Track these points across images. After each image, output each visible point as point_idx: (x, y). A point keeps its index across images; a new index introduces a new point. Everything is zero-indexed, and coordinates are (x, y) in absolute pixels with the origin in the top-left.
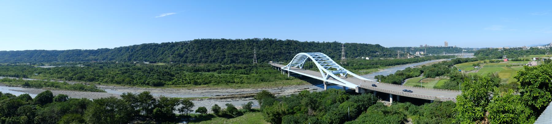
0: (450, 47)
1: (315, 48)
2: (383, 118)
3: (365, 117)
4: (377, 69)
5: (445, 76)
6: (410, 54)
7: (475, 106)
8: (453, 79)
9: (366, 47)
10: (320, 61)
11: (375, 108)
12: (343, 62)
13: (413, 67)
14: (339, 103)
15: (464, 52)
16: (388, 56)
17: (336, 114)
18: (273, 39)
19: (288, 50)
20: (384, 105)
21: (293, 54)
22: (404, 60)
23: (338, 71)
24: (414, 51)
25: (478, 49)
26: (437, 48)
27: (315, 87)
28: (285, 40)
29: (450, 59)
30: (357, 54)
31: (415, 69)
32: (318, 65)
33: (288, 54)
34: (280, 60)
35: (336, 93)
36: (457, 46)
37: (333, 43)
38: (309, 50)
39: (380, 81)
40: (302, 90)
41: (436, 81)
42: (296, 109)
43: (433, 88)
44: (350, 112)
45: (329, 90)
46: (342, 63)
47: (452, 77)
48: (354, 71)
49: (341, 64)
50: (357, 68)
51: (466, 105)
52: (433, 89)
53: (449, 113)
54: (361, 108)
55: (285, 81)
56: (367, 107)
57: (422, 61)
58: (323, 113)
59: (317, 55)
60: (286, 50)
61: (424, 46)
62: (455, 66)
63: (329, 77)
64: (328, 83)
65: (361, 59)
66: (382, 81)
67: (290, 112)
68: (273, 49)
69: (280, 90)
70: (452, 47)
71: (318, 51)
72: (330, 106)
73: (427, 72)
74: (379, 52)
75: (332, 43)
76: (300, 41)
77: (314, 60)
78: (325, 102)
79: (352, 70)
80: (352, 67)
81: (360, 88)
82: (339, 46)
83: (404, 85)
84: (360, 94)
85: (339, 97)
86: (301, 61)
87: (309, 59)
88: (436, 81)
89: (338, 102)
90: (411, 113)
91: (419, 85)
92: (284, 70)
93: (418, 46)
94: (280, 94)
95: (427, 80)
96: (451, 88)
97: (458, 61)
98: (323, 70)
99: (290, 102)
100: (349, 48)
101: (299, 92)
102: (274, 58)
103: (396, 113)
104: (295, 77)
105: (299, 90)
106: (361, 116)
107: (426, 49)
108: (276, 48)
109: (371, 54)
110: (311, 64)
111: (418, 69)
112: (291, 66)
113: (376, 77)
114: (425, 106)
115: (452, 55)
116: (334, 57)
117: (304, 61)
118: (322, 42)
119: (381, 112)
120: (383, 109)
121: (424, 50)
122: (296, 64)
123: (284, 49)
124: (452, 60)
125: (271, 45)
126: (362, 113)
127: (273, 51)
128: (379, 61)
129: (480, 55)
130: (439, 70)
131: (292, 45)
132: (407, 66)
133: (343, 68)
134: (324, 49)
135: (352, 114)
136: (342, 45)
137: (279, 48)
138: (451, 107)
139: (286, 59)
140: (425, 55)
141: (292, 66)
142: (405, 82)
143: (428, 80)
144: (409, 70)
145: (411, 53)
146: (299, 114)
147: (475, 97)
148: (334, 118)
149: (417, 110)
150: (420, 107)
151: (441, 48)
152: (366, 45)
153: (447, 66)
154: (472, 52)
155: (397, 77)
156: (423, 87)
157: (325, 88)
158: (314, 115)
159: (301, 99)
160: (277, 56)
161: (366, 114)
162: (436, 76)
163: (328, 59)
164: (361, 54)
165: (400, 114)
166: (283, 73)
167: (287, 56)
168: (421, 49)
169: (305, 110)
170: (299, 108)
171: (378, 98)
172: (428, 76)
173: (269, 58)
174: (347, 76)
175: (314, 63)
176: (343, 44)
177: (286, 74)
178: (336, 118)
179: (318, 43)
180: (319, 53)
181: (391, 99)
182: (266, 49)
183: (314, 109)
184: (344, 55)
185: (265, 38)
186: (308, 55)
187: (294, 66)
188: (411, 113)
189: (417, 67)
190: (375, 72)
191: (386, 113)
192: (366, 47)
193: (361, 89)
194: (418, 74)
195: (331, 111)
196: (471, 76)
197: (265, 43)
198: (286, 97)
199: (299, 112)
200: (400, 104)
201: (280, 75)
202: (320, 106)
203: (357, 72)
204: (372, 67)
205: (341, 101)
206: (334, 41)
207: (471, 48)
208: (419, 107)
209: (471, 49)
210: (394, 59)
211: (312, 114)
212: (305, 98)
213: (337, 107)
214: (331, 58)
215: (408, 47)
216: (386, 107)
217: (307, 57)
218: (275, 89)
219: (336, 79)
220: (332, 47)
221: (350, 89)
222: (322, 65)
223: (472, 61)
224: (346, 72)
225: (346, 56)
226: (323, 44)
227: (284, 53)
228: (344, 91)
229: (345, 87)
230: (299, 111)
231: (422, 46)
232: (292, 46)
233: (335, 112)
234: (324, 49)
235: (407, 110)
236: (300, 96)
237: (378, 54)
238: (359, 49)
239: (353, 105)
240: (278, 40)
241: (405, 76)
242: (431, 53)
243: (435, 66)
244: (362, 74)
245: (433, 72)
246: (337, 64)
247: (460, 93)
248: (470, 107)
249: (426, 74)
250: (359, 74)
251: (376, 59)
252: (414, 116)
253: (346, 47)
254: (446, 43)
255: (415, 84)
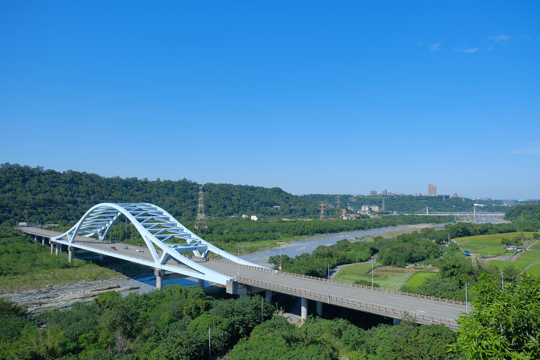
0: (441, 197)
1: (138, 193)
2: (285, 353)
3: (246, 349)
4: (274, 241)
5: (428, 264)
6: (348, 211)
7: (510, 347)
8: (448, 272)
9: (251, 193)
10: (147, 222)
11: (267, 328)
12: (200, 225)
13: (354, 238)
14: (189, 318)
15: (479, 209)
16: (298, 214)
17: (180, 344)
18: (33, 166)
19: (72, 196)
20: (288, 324)
21: (84, 206)
22: (334, 224)
23: (189, 245)
24: (358, 204)
25: (516, 201)
26: (411, 197)
27: (134, 283)
28: (66, 170)
29: (443, 225)
30: (231, 209)
31: (357, 244)
32: (144, 232)
33: (69, 205)
34: (49, 219)
35: (184, 296)
36: (460, 195)
37: (179, 182)
38: (124, 197)
39: (280, 268)
40: (101, 292)
41: (407, 275)
42: (86, 338)
43: (400, 290)
44: (213, 338)
45: (168, 289)
46: (197, 228)
47: (446, 269)
48: (223, 245)
49: (195, 230)
50: (232, 239)
51: (486, 340)
52: (400, 292)
53: (439, 354)
54: (238, 330)
55: (58, 272)
56: (251, 326)
57: (376, 227)
58: (152, 343)
59: (141, 210)
60: (66, 196)
61: (379, 192)
62: (454, 241)
63: (168, 258)
64: (166, 273)
65: (240, 218)
66: (284, 269)
67: (68, 348)
68: (31, 191)
69: (45, 295)
70: (447, 197)
71: (145, 199)
72: (167, 327)
73: (387, 252)
74: (279, 205)
75: (176, 183)
76: (102, 176)
77: (133, 220)
78: (158, 318)
79: (219, 243)
80: (220, 237)
81: (235, 284)
82: (192, 189)
83: (334, 279)
84: (235, 296)
85: (191, 303)
86: (103, 221)
87: (123, 219)
88: (407, 275)
89: (186, 316)
90: (348, 344)
91: (367, 280)
92: (59, 244)
93: (366, 193)
94: (43, 306)
95: (386, 271)
96: (445, 294)
97: (461, 231)
98: (153, 244)
99: (70, 324)
100: (215, 194)
101: (95, 296)
102: (30, 214)
103: (314, 342)
104: (85, 261)
105: (95, 293)
106: (237, 347)
107: (386, 200)
108: (39, 189)
109: (262, 208)
110: (128, 229)
111: (365, 245)
112: (76, 234)
113: (274, 261)
114: (380, 331)
115: (447, 214)
116: (181, 213)
117: (111, 222)
118: (155, 180)
119: (280, 338)
120: (285, 333)
121: (381, 202)
122: (91, 229)
123: (60, 194)
124: (446, 227)
125: (24, 181)
126: (238, 340)
127: (31, 196)
128: (281, 224)
129: (521, 219)
130: (415, 248)
131: (82, 184)
132: (341, 236)
133: (200, 239)
134: (158, 196)
135: (218, 345)
136: (198, 188)
137: (49, 190)
138: (444, 339)
139: (65, 218)
140: (382, 213)
141: (80, 235)
142: (335, 271)
143: (389, 271)
144: (345, 245)
145: (349, 208)
146: (92, 352)
147: (510, 325)
148: (176, 354)
149: (362, 339)
150: (369, 332)
151: (420, 198)
152: (253, 188)
153: (434, 241)
154: (498, 209)
155: (318, 261)
156: (376, 286)
157: (158, 285)
158: (130, 351)
159: (100, 314)
160: (40, 210)
161: (248, 343)
162: (407, 263)
163: (167, 219)
164: (241, 208)
165: (322, 346)
166: (54, 251)
167: (69, 209)
168: (372, 200)
169: (109, 340)
170: (94, 336)
171: (275, 306)
172: (389, 263)
173: (16, 215)
174: (208, 256)
175: (134, 227)
176: (201, 185)
177: (65, 254)
178: (181, 355)
179: (146, 182)
180: (147, 204)
181: (304, 310)
182: (9, 190)
183: (130, 335)
184: (203, 211)
185: (118, 177)
186: (121, 209)
187: (84, 234)
188: (348, 344)
189: (363, 240)
190: (271, 249)
191: (291, 341)
192: (251, 193)
193: (239, 285)
194: (365, 254)
195: (170, 338)
196: (497, 269)
197: (8, 175)
198: (61, 310)
199: (92, 345)
200: (324, 323)
201: (48, 256)
202: (144, 327)
203: (230, 248)
204: (265, 237)
205: (194, 313)
206: (181, 179)
207: (495, 201)
208: (365, 332)
209: (496, 201)
210: (312, 221)
211: (126, 349)
212: (109, 309)
213: (184, 328)
214: (174, 216)
215: (342, 194)
216: (293, 327)
217: (117, 213)
218: (29, 294)
219: (183, 264)
220: (176, 191)
221: (212, 286)
222: (153, 233)
223: (500, 232)
224: (206, 248)
225: (207, 210)
226: (158, 184)
227: (59, 201)
228: (201, 291)
229: (202, 282)
230: (93, 342)
231: (376, 192)
232: (81, 187)
233: (178, 340)
234: (158, 196)
235: (340, 338)
236: (97, 306)
237: (277, 209)
238: (235, 198)
239: (220, 322)
240: (45, 169)
241: (336, 259)
242: (396, 210)
243: (404, 239)
244: (240, 252)
245: (401, 254)
246: (186, 230)
247: (468, 309)
248: (497, 347)
249: (385, 256)
250: (236, 253)
251: (273, 221)
252: (354, 352)
253: (207, 193)
254: (432, 188)
255: (359, 278)
